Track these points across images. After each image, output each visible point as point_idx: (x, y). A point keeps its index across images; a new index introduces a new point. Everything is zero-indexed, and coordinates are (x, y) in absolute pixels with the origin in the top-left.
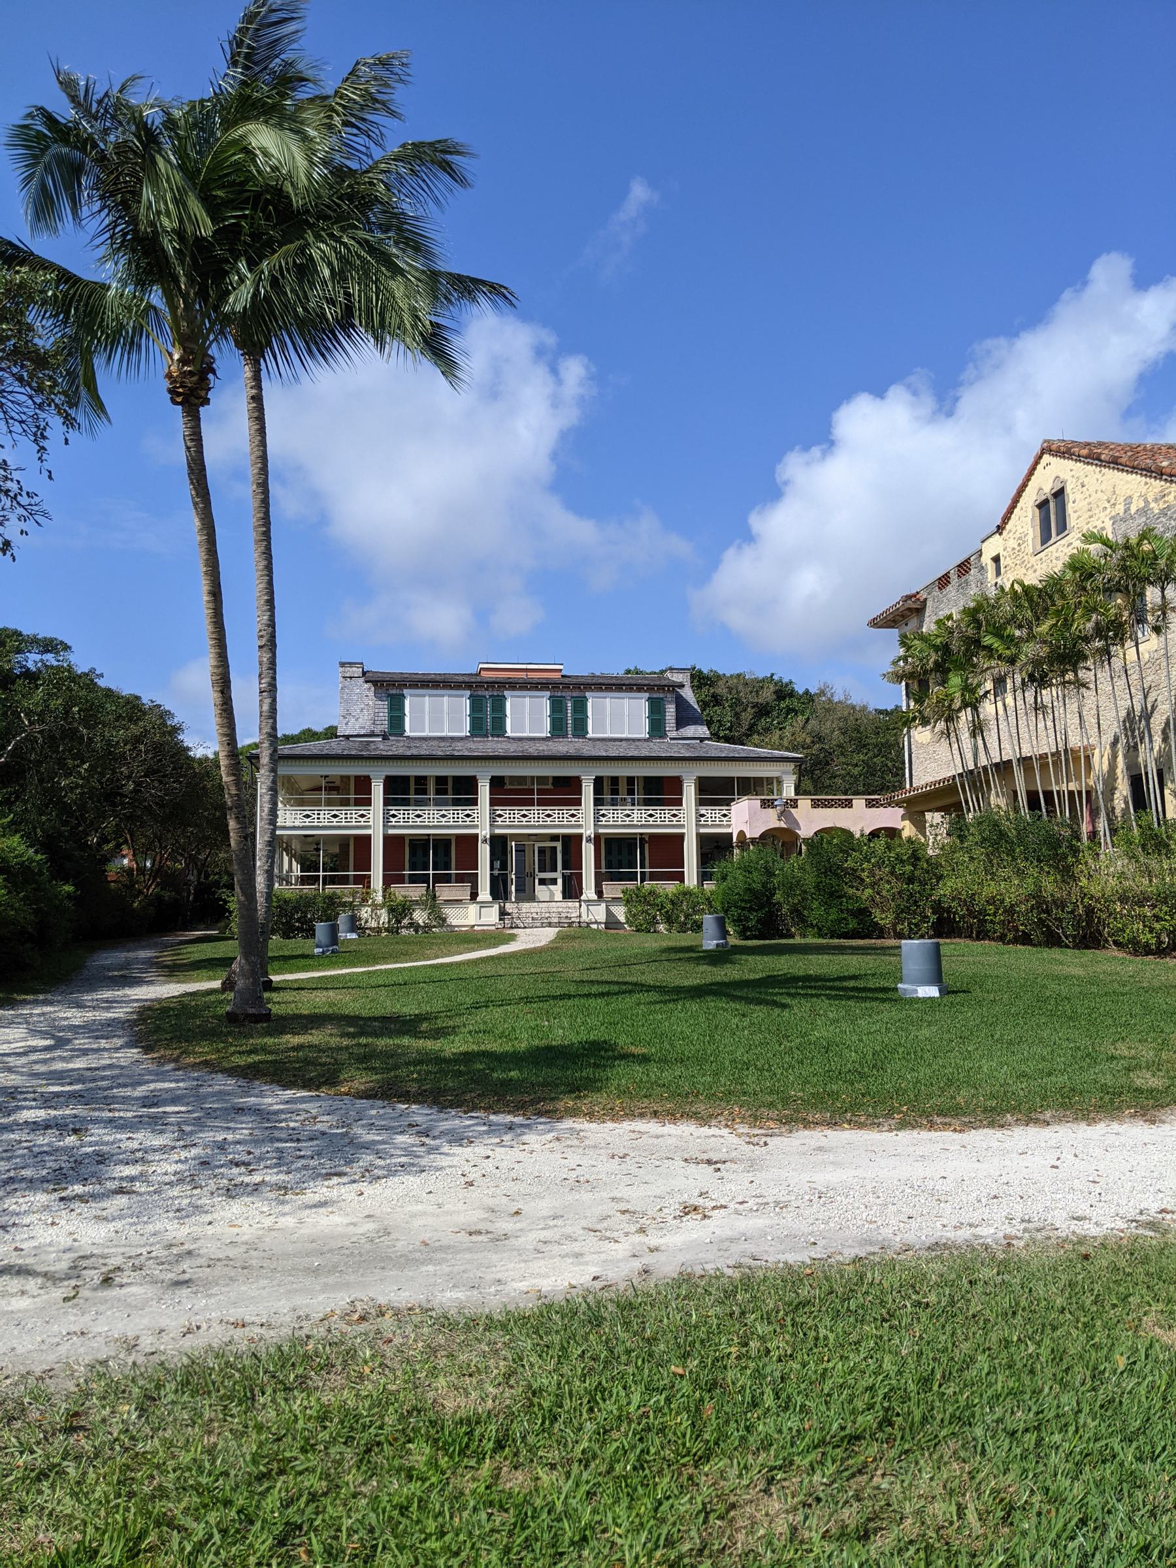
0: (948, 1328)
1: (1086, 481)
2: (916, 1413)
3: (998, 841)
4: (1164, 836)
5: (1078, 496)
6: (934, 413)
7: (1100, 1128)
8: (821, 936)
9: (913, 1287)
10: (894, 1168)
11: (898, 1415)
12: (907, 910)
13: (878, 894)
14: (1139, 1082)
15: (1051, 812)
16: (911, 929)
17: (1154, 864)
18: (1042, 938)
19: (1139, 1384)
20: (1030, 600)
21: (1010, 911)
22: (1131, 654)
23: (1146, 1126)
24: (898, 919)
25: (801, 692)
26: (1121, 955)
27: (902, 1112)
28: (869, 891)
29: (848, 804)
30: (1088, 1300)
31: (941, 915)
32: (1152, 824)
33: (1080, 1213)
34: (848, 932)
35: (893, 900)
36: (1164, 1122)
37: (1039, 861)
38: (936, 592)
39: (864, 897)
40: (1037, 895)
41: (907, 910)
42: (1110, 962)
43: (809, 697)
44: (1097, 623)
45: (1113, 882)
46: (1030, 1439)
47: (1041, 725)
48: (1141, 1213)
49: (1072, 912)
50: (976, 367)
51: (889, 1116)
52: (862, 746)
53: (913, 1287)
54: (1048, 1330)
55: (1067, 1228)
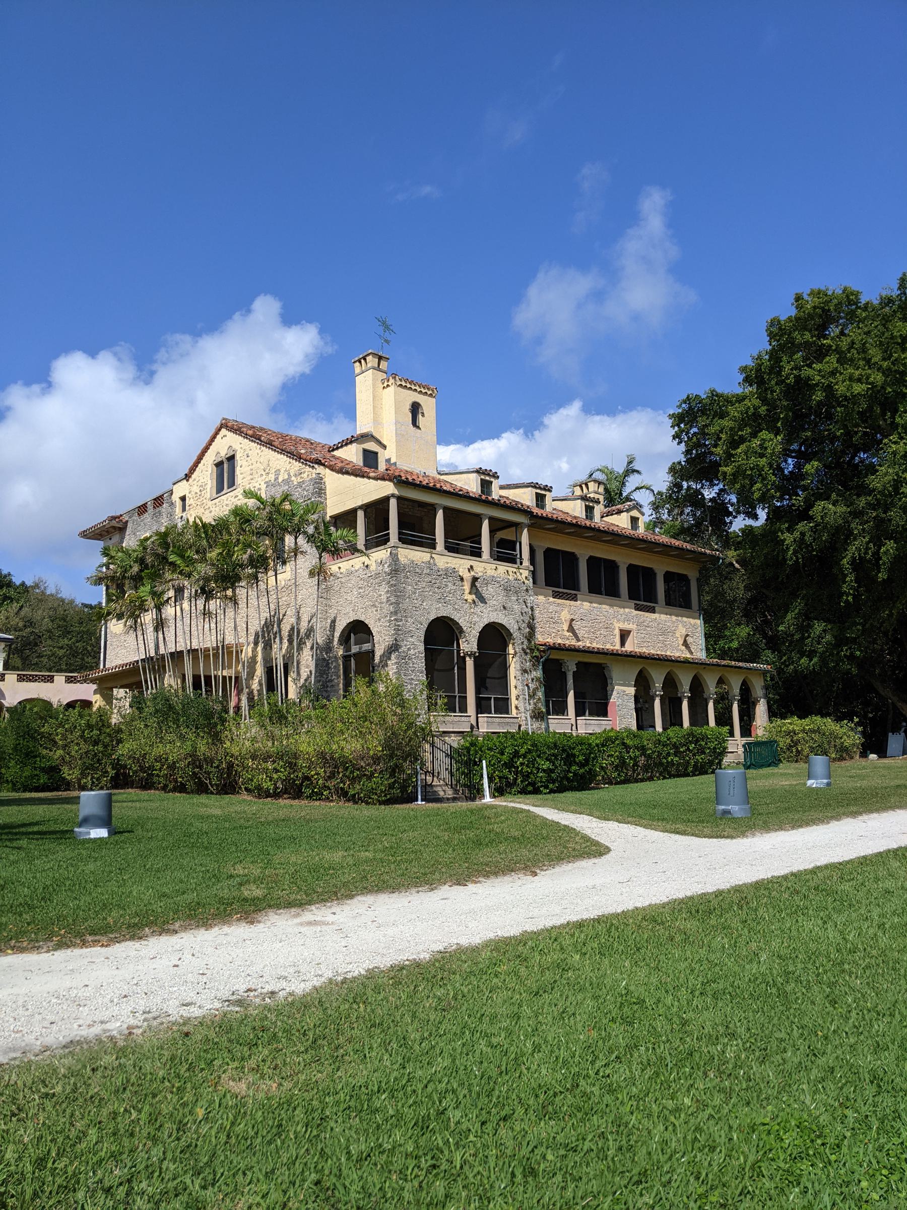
0: (68, 1111)
1: (250, 453)
2: (28, 1191)
3: (168, 712)
4: (285, 711)
5: (244, 463)
6: (134, 379)
7: (215, 931)
8: (15, 790)
9: (43, 1082)
10: (46, 983)
11: (13, 1196)
12: (92, 767)
13: (66, 754)
14: (246, 893)
15: (209, 692)
16: (93, 782)
17: (277, 732)
18: (194, 787)
19: (211, 1127)
20: (206, 532)
21: (172, 767)
22: (272, 581)
23: (247, 926)
24: (83, 775)
25: (18, 583)
26: (250, 798)
27: (60, 935)
28: (60, 752)
29: (51, 679)
30: (183, 1070)
31: (118, 770)
32: (277, 702)
33: (189, 1000)
34: (38, 787)
35: (80, 759)
36: (259, 922)
37: (197, 728)
38: (136, 517)
39: (56, 757)
40: (193, 755)
41: (92, 767)
42: (242, 804)
43: (24, 589)
44: (251, 556)
45: (248, 744)
46: (121, 1192)
47: (207, 626)
48: (233, 994)
49: (217, 767)
50: (167, 352)
51: (49, 939)
52: (66, 632)
53: (43, 1082)
54: (149, 1098)
55: (176, 1012)
